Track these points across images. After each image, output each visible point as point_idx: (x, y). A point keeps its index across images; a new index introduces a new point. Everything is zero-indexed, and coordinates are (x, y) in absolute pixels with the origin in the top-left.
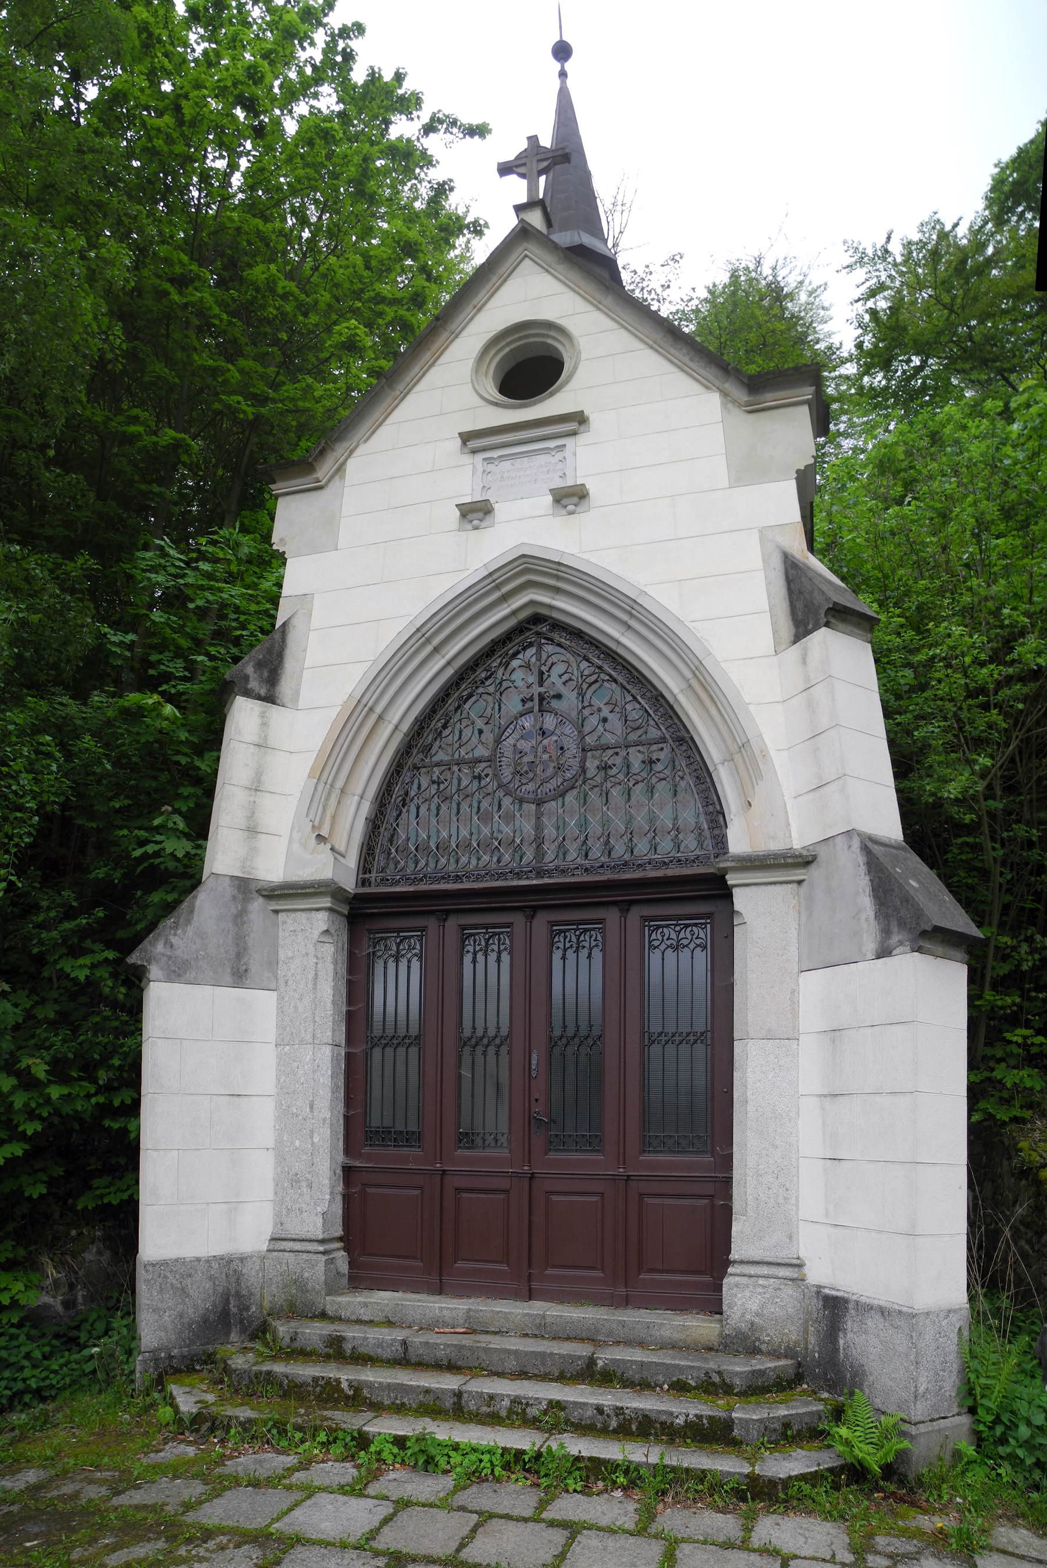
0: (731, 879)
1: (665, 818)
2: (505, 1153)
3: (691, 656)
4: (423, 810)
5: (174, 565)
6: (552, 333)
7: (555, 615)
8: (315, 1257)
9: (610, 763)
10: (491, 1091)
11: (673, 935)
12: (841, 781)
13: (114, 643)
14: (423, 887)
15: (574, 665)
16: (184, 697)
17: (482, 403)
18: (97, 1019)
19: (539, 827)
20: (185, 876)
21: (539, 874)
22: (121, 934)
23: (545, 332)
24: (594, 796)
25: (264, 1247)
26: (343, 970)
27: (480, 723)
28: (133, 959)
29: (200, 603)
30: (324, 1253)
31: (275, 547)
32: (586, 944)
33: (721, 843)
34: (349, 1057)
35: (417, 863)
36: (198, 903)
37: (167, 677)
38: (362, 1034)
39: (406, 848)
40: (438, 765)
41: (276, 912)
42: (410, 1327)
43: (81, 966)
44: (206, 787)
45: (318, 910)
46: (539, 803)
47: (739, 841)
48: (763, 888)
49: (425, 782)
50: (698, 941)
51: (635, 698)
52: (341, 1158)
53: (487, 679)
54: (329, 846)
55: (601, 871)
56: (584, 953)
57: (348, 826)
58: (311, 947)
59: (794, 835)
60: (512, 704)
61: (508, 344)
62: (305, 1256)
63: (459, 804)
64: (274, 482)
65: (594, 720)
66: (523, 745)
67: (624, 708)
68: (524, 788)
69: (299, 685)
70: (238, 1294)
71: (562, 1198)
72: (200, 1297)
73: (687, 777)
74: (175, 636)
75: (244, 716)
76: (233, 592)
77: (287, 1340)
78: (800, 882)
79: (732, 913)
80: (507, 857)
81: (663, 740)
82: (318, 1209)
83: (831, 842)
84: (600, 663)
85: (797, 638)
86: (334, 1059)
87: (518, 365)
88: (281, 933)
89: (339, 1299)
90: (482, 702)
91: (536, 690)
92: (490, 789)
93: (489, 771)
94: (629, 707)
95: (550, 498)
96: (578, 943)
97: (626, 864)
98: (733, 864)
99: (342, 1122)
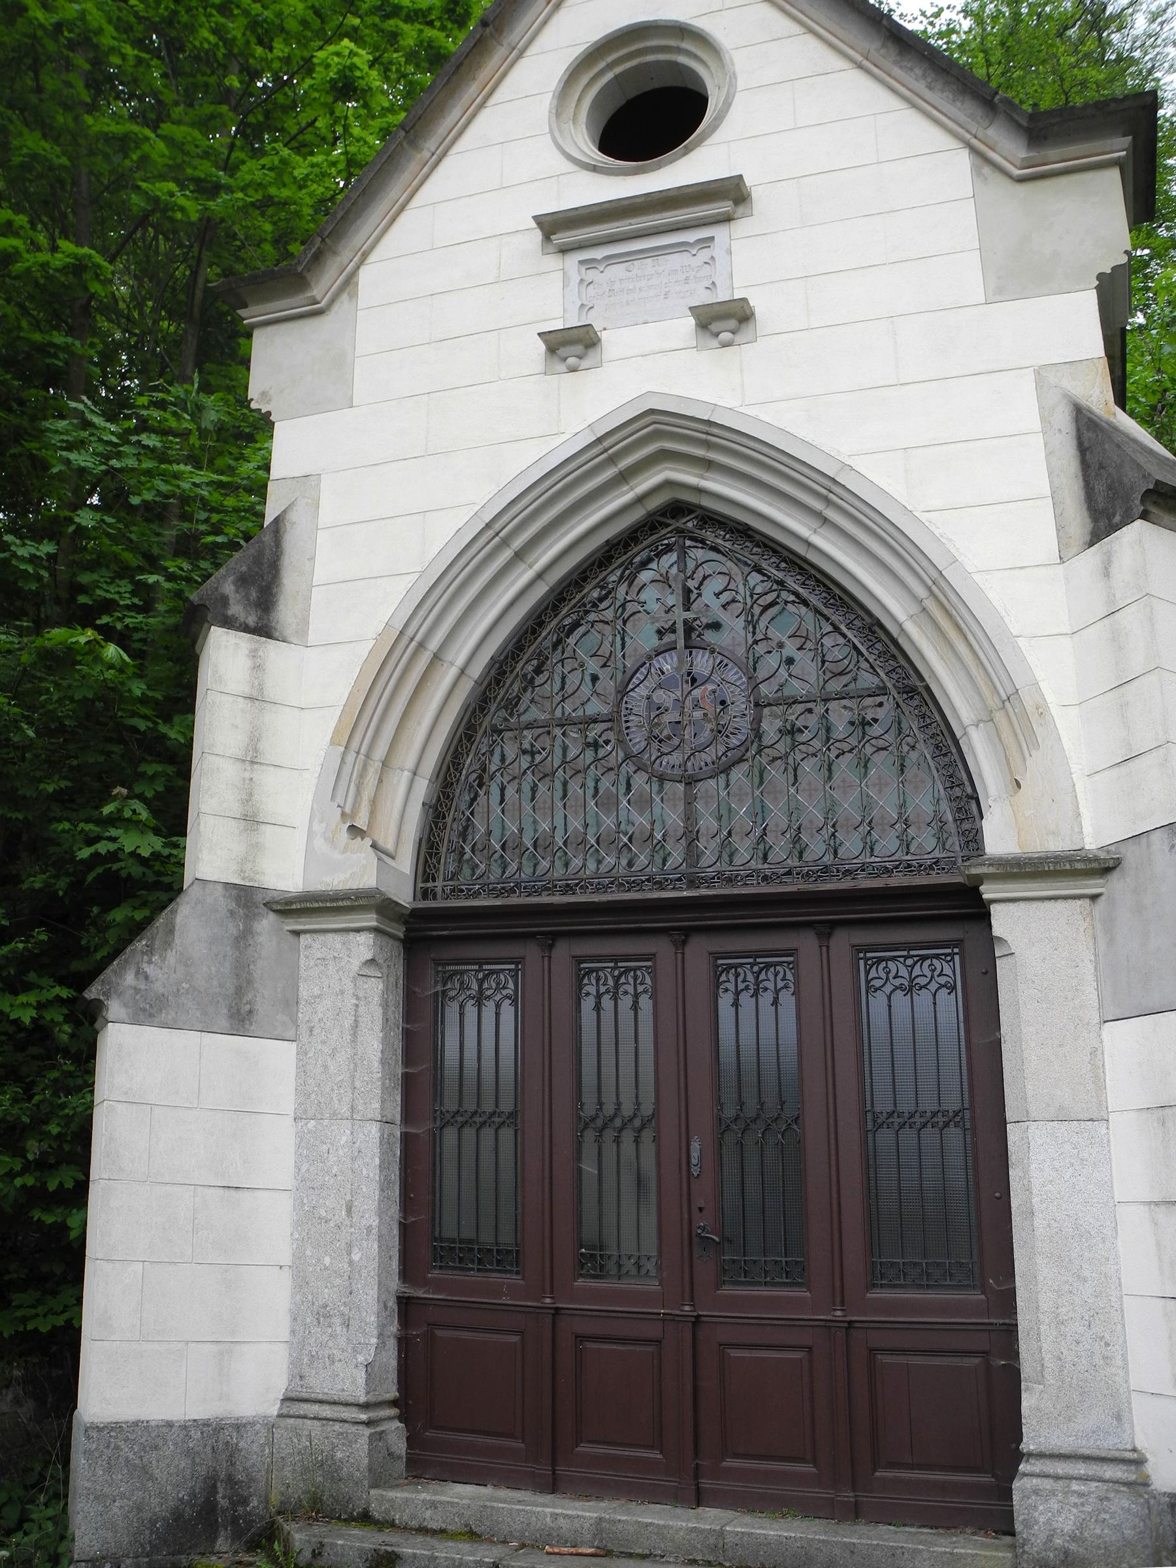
0: (988, 892)
1: (886, 805)
2: (654, 1286)
3: (925, 563)
4: (510, 791)
5: (100, 440)
6: (685, 45)
7: (706, 502)
8: (353, 1429)
9: (799, 724)
10: (628, 1181)
11: (903, 972)
12: (1162, 751)
13: (22, 559)
14: (514, 900)
15: (739, 579)
16: (137, 636)
17: (569, 167)
18: (55, 1074)
19: (690, 817)
20: (157, 886)
21: (692, 883)
22: (77, 966)
23: (672, 43)
24: (775, 773)
25: (274, 1410)
26: (397, 1015)
27: (593, 666)
28: (92, 993)
29: (148, 496)
30: (368, 1423)
31: (253, 405)
32: (770, 985)
33: (973, 840)
34: (406, 1139)
35: (504, 867)
36: (179, 919)
37: (108, 606)
38: (428, 1105)
39: (487, 846)
40: (530, 726)
41: (297, 933)
42: (505, 1542)
43: (24, 1005)
44: (179, 761)
45: (358, 930)
46: (690, 781)
47: (1000, 836)
48: (1036, 904)
49: (511, 751)
50: (943, 980)
51: (836, 629)
52: (394, 1284)
53: (601, 599)
54: (368, 842)
55: (785, 879)
56: (766, 998)
57: (396, 814)
58: (348, 985)
59: (1087, 829)
60: (644, 637)
61: (610, 67)
62: (337, 1427)
63: (565, 784)
64: (245, 306)
65: (772, 661)
66: (660, 696)
67: (819, 642)
68: (665, 760)
69: (307, 610)
70: (231, 1480)
71: (746, 1354)
72: (171, 1482)
73: (921, 746)
74: (117, 549)
75: (225, 656)
76: (194, 479)
77: (307, 1554)
78: (1094, 898)
79: (990, 941)
80: (642, 860)
81: (882, 690)
82: (357, 1358)
83: (1144, 839)
84: (780, 575)
85: (1095, 538)
86: (384, 1142)
87: (629, 103)
88: (302, 962)
89: (391, 1494)
90: (594, 636)
91: (680, 615)
92: (612, 761)
93: (610, 735)
94: (828, 642)
95: (692, 321)
96: (757, 983)
97: (826, 869)
98: (991, 870)
99: (396, 1231)
